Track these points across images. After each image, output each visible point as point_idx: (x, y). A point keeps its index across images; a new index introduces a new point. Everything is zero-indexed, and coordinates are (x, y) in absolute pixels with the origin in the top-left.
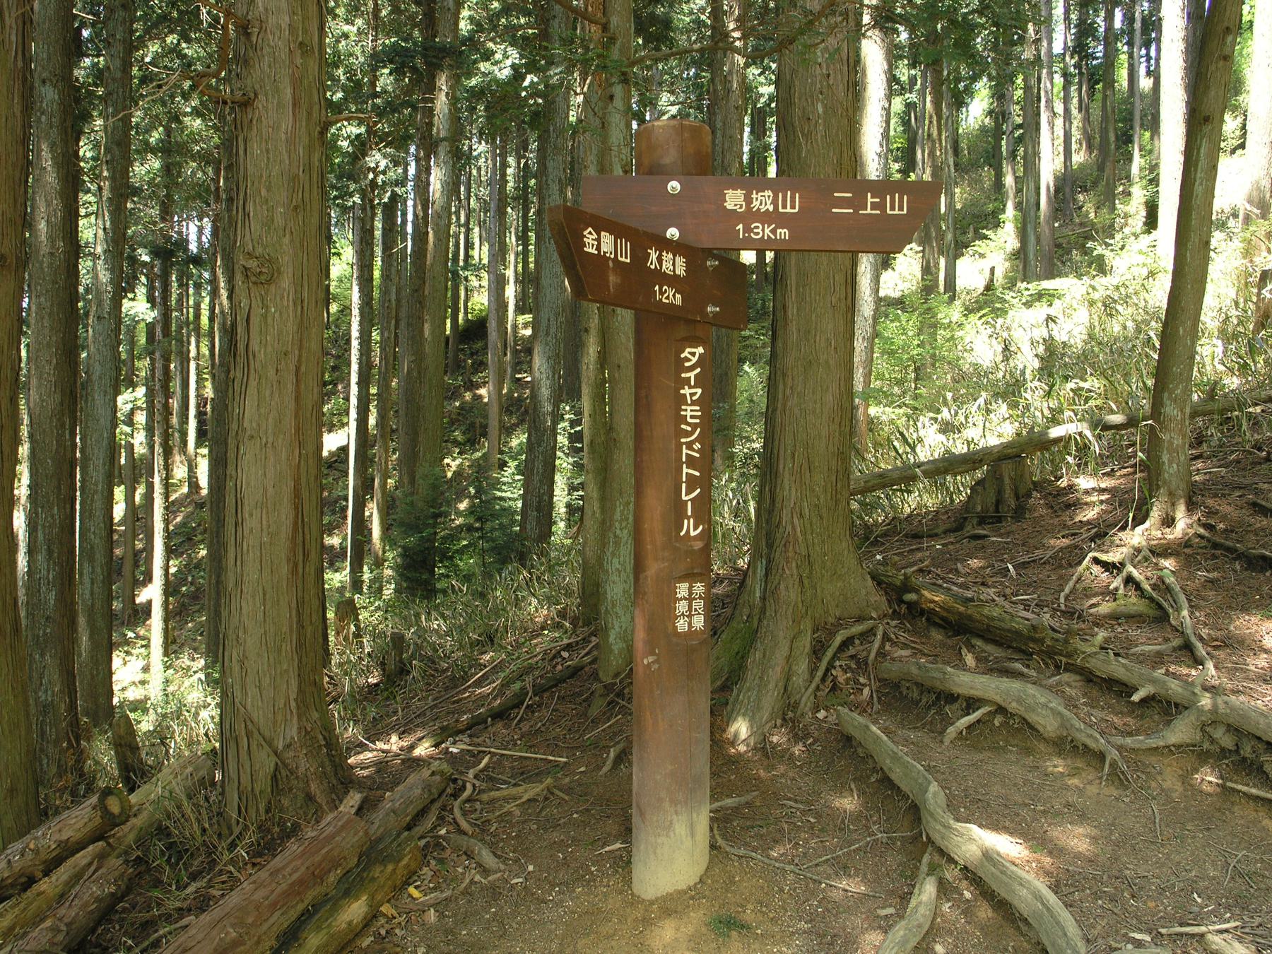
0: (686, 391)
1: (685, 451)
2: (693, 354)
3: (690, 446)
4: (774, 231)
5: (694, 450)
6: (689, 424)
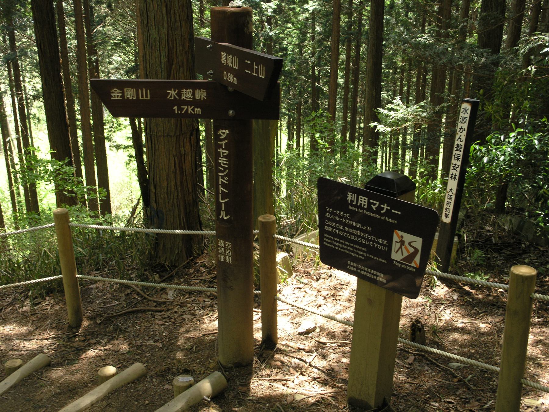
0: (220, 150)
1: (221, 180)
2: (224, 133)
3: (223, 177)
4: (193, 110)
5: (224, 180)
6: (222, 167)
